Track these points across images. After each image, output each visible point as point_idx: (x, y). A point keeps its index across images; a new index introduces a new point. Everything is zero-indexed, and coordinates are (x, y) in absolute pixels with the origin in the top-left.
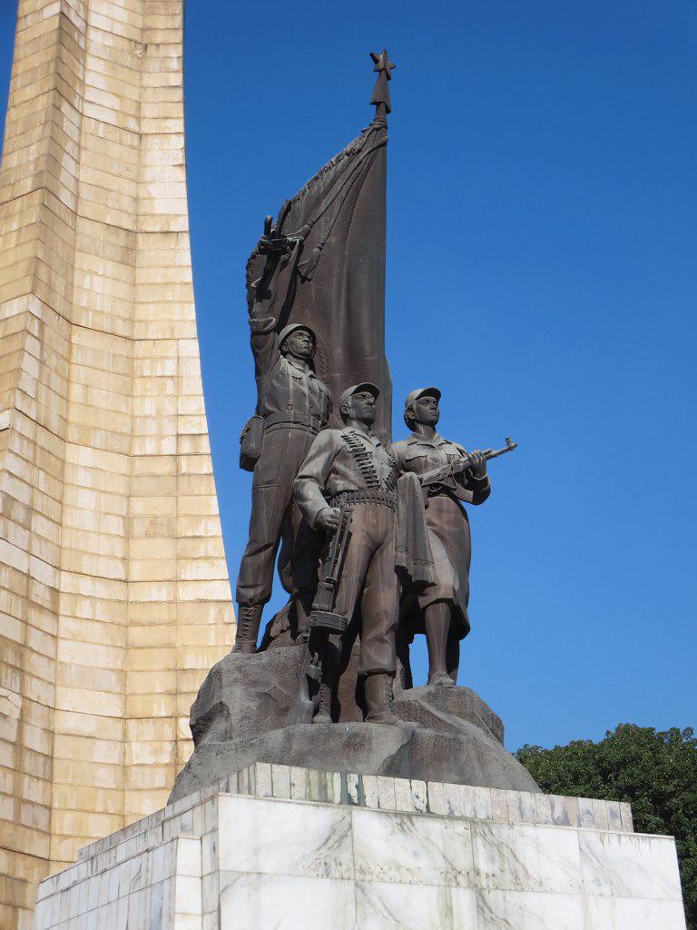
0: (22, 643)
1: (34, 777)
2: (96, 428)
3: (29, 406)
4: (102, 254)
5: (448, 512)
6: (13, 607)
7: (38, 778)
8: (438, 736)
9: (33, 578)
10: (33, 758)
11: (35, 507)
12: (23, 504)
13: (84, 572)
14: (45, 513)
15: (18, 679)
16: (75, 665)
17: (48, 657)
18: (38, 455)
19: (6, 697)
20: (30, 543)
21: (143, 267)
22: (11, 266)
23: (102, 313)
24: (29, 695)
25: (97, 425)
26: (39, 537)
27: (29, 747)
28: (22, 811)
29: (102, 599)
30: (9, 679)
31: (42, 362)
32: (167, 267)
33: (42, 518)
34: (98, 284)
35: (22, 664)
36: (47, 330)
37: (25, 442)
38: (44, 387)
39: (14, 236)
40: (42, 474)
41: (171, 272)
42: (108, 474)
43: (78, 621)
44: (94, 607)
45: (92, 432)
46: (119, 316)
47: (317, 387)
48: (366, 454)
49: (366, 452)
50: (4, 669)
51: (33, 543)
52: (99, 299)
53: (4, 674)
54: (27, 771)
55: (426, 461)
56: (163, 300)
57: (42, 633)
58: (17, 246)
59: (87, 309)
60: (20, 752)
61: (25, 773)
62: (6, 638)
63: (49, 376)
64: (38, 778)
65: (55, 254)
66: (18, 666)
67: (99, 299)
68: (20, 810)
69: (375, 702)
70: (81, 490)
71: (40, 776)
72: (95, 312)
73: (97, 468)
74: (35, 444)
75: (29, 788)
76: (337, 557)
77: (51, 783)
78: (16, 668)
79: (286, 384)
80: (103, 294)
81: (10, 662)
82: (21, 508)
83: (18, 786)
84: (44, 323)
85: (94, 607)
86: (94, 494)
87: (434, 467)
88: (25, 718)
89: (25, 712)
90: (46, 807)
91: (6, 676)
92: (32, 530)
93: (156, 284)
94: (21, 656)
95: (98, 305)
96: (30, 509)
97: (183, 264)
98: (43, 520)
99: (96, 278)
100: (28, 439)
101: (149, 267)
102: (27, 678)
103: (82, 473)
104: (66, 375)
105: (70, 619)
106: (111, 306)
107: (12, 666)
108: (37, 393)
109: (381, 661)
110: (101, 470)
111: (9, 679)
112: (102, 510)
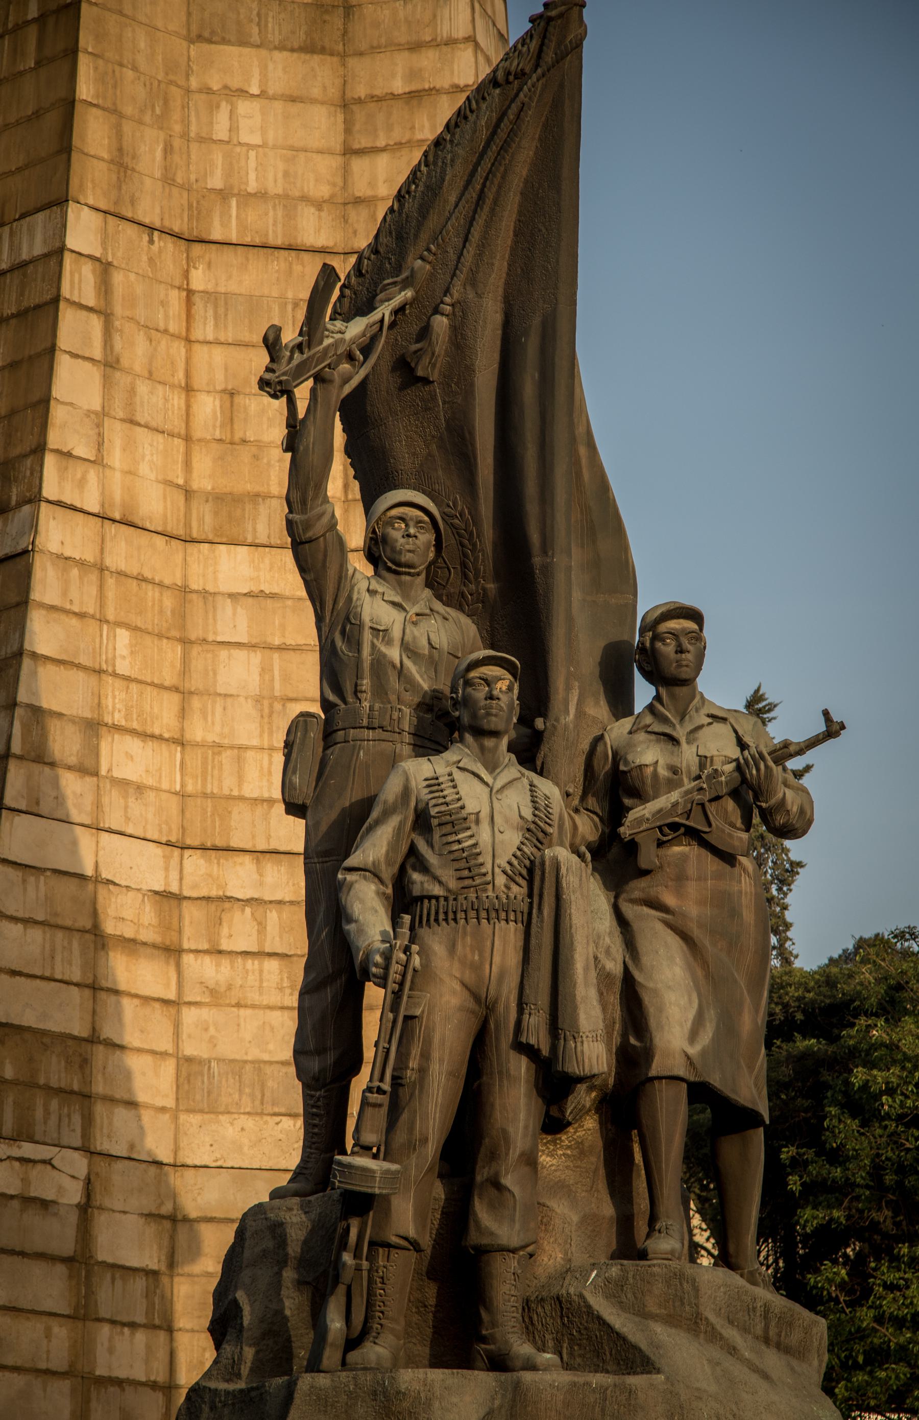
0: (85, 1034)
1: (124, 1325)
2: (257, 495)
3: (82, 483)
4: (256, 39)
5: (699, 879)
6: (58, 958)
7: (133, 1325)
8: (574, 1384)
9: (109, 882)
10: (119, 1283)
11: (108, 719)
12: (73, 720)
13: (234, 844)
14: (135, 725)
15: (77, 1119)
16: (219, 1060)
17: (153, 1052)
18: (111, 594)
19: (48, 1162)
20: (98, 805)
21: (361, 54)
22: (29, 119)
23: (262, 195)
24: (103, 1144)
25: (258, 488)
26: (123, 784)
27: (110, 1260)
28: (94, 1404)
29: (280, 902)
30: (54, 1119)
31: (110, 364)
32: (415, 47)
33: (128, 739)
34: (251, 122)
35: (87, 1081)
36: (118, 278)
37: (75, 572)
38: (118, 426)
39: (32, 33)
40: (123, 637)
41: (427, 59)
42: (289, 603)
43: (225, 962)
44: (262, 926)
45: (248, 507)
46: (305, 199)
47: (425, 642)
48: (465, 819)
49: (464, 813)
50: (39, 1102)
51: (105, 800)
52: (252, 163)
53: (39, 1113)
54: (103, 1313)
55: (655, 774)
56: (409, 142)
57: (136, 1001)
58: (38, 63)
59: (223, 195)
60: (88, 1277)
61: (99, 1320)
62: (44, 1033)
63: (132, 392)
64: (133, 1325)
65: (129, 74)
66: (76, 1087)
67: (252, 163)
68: (87, 1401)
69: (487, 1309)
70: (223, 653)
71: (140, 1319)
72: (246, 198)
73: (261, 595)
74: (102, 569)
75: (111, 1350)
76: (390, 1042)
77: (170, 1330)
78: (72, 1092)
79: (357, 646)
80: (264, 145)
81: (54, 1084)
82: (70, 729)
83: (82, 1349)
84: (110, 264)
85: (262, 926)
86: (256, 658)
87: (672, 784)
88: (98, 1199)
89: (97, 1186)
90: (154, 1386)
91: (47, 1113)
92: (103, 772)
93: (394, 97)
94: (85, 1063)
95: (252, 176)
96: (93, 727)
97: (455, 35)
98: (133, 745)
99: (244, 107)
100: (81, 564)
101: (375, 49)
102: (99, 1109)
103: (226, 608)
104: (181, 375)
105: (207, 959)
106: (286, 174)
107: (60, 1091)
108: (100, 445)
109: (499, 1232)
110: (273, 596)
111: (54, 1119)
112: (277, 694)
